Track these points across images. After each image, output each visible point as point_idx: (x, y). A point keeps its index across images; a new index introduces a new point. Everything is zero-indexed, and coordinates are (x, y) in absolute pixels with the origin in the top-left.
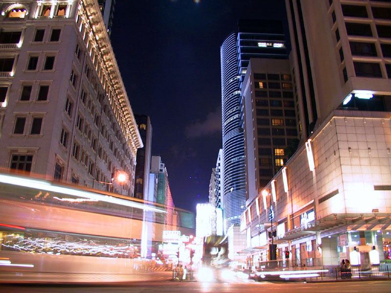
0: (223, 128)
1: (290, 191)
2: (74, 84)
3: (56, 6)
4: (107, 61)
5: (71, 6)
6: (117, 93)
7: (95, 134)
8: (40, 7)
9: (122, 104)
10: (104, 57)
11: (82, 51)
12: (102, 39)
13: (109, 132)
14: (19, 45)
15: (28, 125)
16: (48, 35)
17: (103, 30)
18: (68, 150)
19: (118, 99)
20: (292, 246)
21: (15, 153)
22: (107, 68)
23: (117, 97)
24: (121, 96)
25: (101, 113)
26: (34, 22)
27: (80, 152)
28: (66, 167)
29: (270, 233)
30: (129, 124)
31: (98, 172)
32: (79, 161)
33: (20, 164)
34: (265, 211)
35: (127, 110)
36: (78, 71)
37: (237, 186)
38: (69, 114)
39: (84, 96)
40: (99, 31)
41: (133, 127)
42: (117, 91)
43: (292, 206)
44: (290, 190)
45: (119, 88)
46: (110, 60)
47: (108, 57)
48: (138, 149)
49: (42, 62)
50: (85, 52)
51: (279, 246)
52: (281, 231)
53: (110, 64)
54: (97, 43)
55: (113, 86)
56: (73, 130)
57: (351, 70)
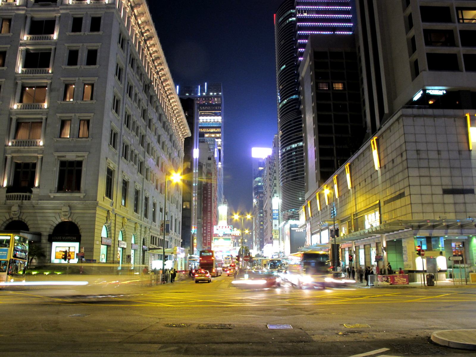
0: (278, 110)
1: (354, 189)
2: (119, 78)
4: (151, 46)
6: (162, 80)
7: (142, 130)
9: (167, 92)
10: (148, 43)
12: (146, 22)
14: (55, 36)
16: (87, 24)
17: (145, 13)
18: (117, 152)
19: (164, 87)
20: (355, 247)
21: (63, 159)
22: (151, 54)
23: (162, 84)
24: (166, 83)
25: (148, 105)
26: (69, 9)
27: (129, 152)
28: (116, 170)
29: (332, 231)
34: (327, 207)
35: (173, 98)
36: (122, 64)
38: (116, 111)
39: (130, 89)
40: (142, 14)
41: (183, 125)
42: (162, 78)
44: (353, 187)
45: (164, 75)
46: (154, 45)
47: (152, 42)
48: (185, 138)
49: (83, 56)
50: (129, 40)
51: (342, 246)
52: (344, 231)
53: (154, 49)
54: (140, 28)
55: (157, 73)
56: (121, 129)
57: (423, 63)
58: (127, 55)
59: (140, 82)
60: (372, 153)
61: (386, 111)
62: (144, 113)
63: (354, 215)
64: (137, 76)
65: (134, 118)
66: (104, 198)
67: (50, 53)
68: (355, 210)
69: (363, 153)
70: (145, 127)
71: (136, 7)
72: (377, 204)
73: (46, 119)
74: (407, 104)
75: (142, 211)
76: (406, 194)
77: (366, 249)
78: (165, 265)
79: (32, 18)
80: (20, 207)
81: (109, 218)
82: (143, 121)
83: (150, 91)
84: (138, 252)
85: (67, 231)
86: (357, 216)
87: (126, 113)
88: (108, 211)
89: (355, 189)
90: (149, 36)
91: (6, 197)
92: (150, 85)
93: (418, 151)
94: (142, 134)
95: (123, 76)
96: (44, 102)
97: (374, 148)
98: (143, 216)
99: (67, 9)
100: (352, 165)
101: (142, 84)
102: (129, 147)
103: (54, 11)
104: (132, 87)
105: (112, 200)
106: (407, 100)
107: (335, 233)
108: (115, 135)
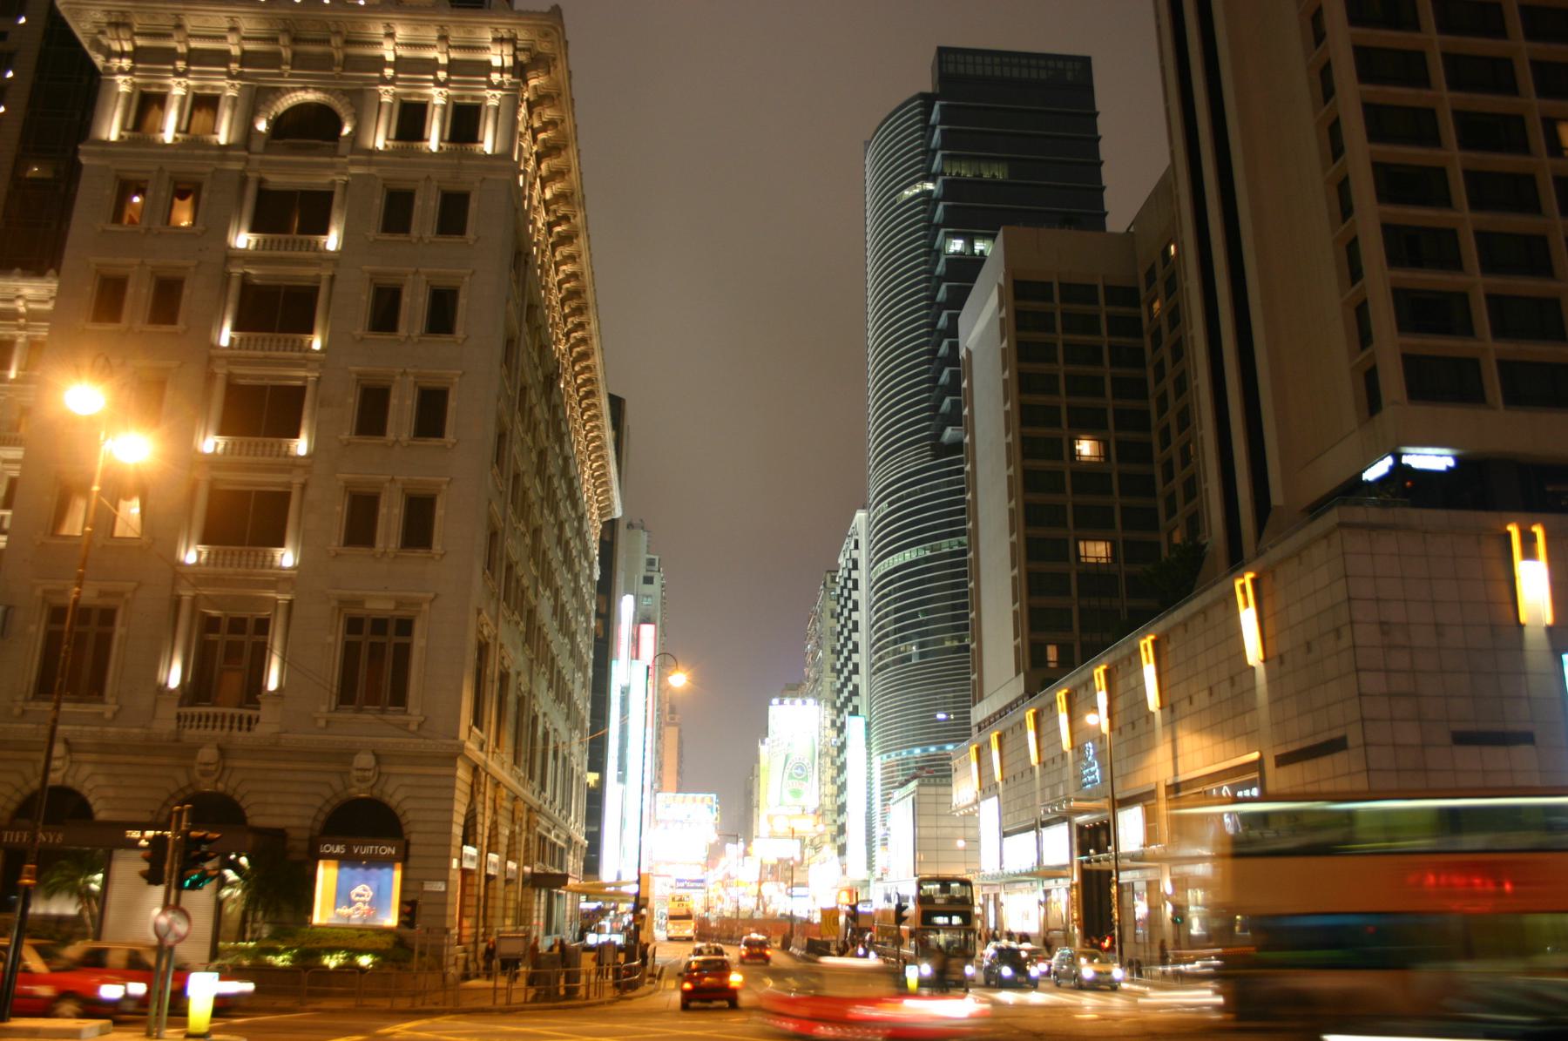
1: (1167, 710)
3: (444, 108)
5: (497, 109)
8: (391, 105)
14: (332, 241)
15: (391, 517)
16: (426, 209)
21: (356, 612)
24: (584, 364)
26: (378, 164)
33: (372, 644)
34: (1064, 755)
43: (1175, 757)
44: (1167, 704)
49: (414, 306)
57: (1393, 382)
60: (1237, 614)
67: (316, 290)
73: (304, 487)
76: (1350, 743)
79: (261, 181)
80: (223, 752)
85: (366, 827)
89: (1172, 711)
91: (179, 717)
93: (1384, 626)
96: (297, 436)
97: (1246, 604)
99: (369, 163)
103: (331, 166)
106: (1344, 476)
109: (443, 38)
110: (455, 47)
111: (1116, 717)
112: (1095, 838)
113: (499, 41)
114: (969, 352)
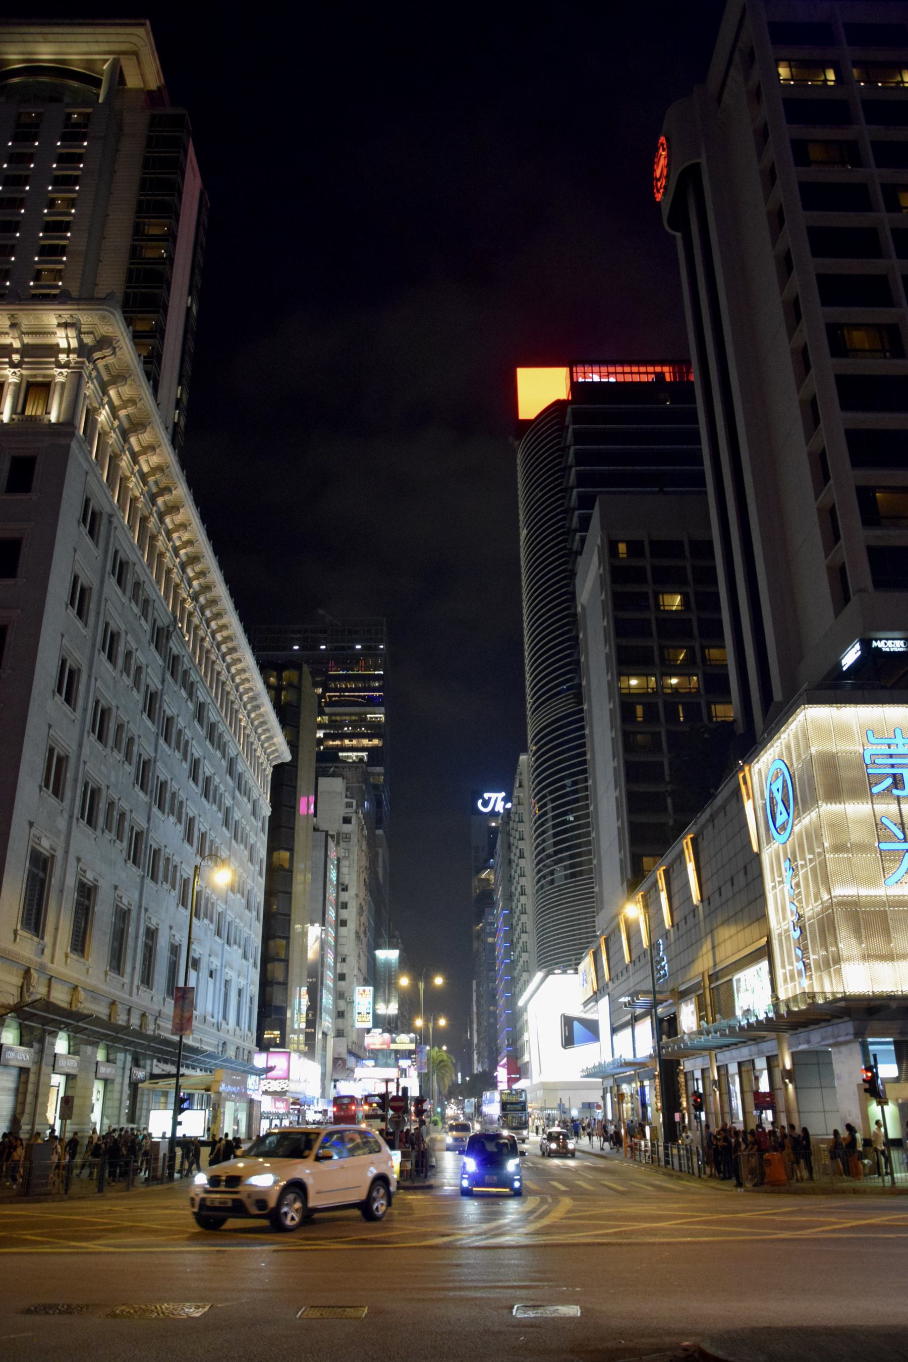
5: (63, 385)
10: (168, 520)
11: (128, 563)
13: (188, 734)
20: (718, 1068)
25: (163, 682)
27: (102, 806)
30: (245, 698)
31: (157, 853)
32: (99, 831)
36: (89, 577)
37: (572, 866)
39: (110, 644)
50: (110, 516)
51: (687, 1065)
52: (688, 1018)
56: (80, 746)
57: (861, 574)
58: (106, 551)
59: (143, 621)
61: (778, 696)
62: (152, 704)
63: (710, 976)
64: (133, 605)
65: (120, 715)
66: (15, 932)
68: (711, 964)
69: (723, 807)
70: (153, 739)
71: (136, 431)
72: (764, 946)
74: (57, 796)
75: (134, 968)
77: (744, 1074)
78: (180, 1123)
81: (28, 991)
82: (149, 723)
83: (171, 644)
84: (117, 1087)
86: (717, 979)
87: (97, 702)
88: (27, 973)
90: (170, 504)
92: (171, 629)
94: (145, 757)
95: (93, 606)
98: (137, 981)
100: (700, 839)
101: (147, 627)
102: (104, 792)
104: (119, 633)
105: (43, 938)
107: (667, 1027)
108: (62, 761)
109: (13, 326)
110: (28, 333)
111: (675, 913)
112: (667, 1027)
113: (66, 325)
114: (583, 608)
